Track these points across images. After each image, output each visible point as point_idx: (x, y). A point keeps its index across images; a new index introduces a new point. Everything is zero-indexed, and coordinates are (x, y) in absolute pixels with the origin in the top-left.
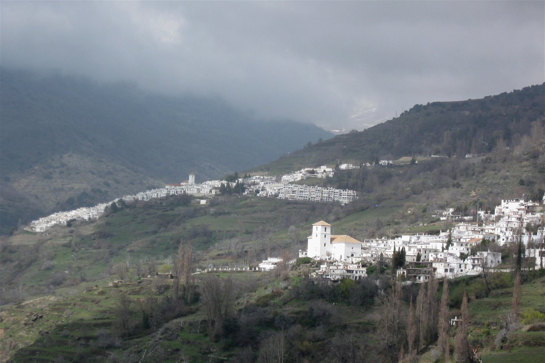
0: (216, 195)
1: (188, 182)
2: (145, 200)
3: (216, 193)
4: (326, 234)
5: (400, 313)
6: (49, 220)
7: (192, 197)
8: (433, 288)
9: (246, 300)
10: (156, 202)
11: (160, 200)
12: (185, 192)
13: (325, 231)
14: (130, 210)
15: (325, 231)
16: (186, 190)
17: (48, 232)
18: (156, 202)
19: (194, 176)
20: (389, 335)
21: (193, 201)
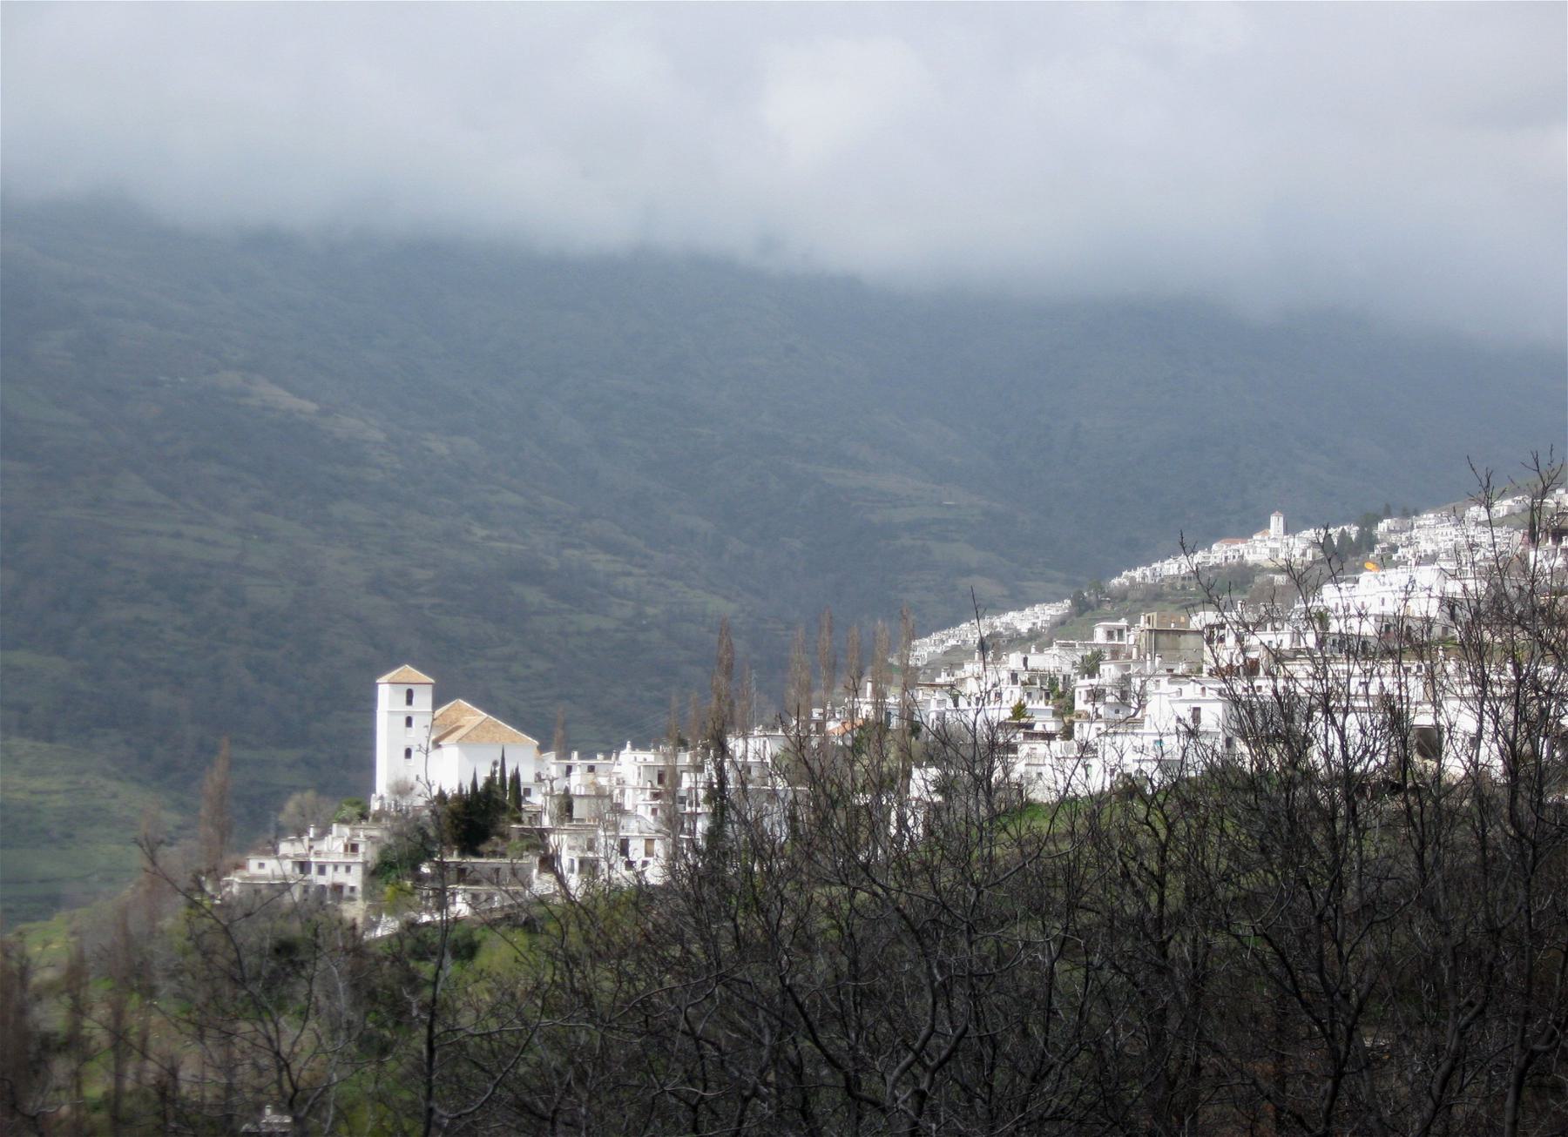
0: (1314, 562)
1: (1268, 534)
2: (1149, 581)
3: (1314, 557)
4: (414, 713)
5: (158, 1114)
6: (944, 637)
7: (1257, 569)
8: (223, 1010)
9: (306, 957)
10: (1172, 586)
11: (1184, 578)
12: (1242, 557)
13: (409, 702)
14: (1113, 608)
15: (409, 702)
16: (1246, 551)
17: (933, 666)
18: (1172, 586)
19: (1281, 519)
20: (631, 1114)
21: (1258, 580)
